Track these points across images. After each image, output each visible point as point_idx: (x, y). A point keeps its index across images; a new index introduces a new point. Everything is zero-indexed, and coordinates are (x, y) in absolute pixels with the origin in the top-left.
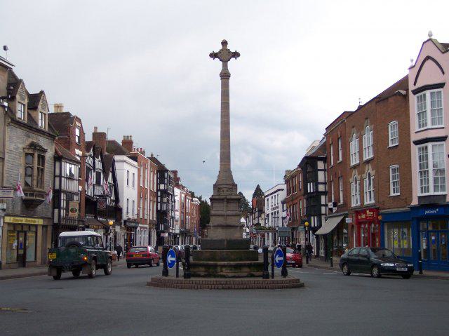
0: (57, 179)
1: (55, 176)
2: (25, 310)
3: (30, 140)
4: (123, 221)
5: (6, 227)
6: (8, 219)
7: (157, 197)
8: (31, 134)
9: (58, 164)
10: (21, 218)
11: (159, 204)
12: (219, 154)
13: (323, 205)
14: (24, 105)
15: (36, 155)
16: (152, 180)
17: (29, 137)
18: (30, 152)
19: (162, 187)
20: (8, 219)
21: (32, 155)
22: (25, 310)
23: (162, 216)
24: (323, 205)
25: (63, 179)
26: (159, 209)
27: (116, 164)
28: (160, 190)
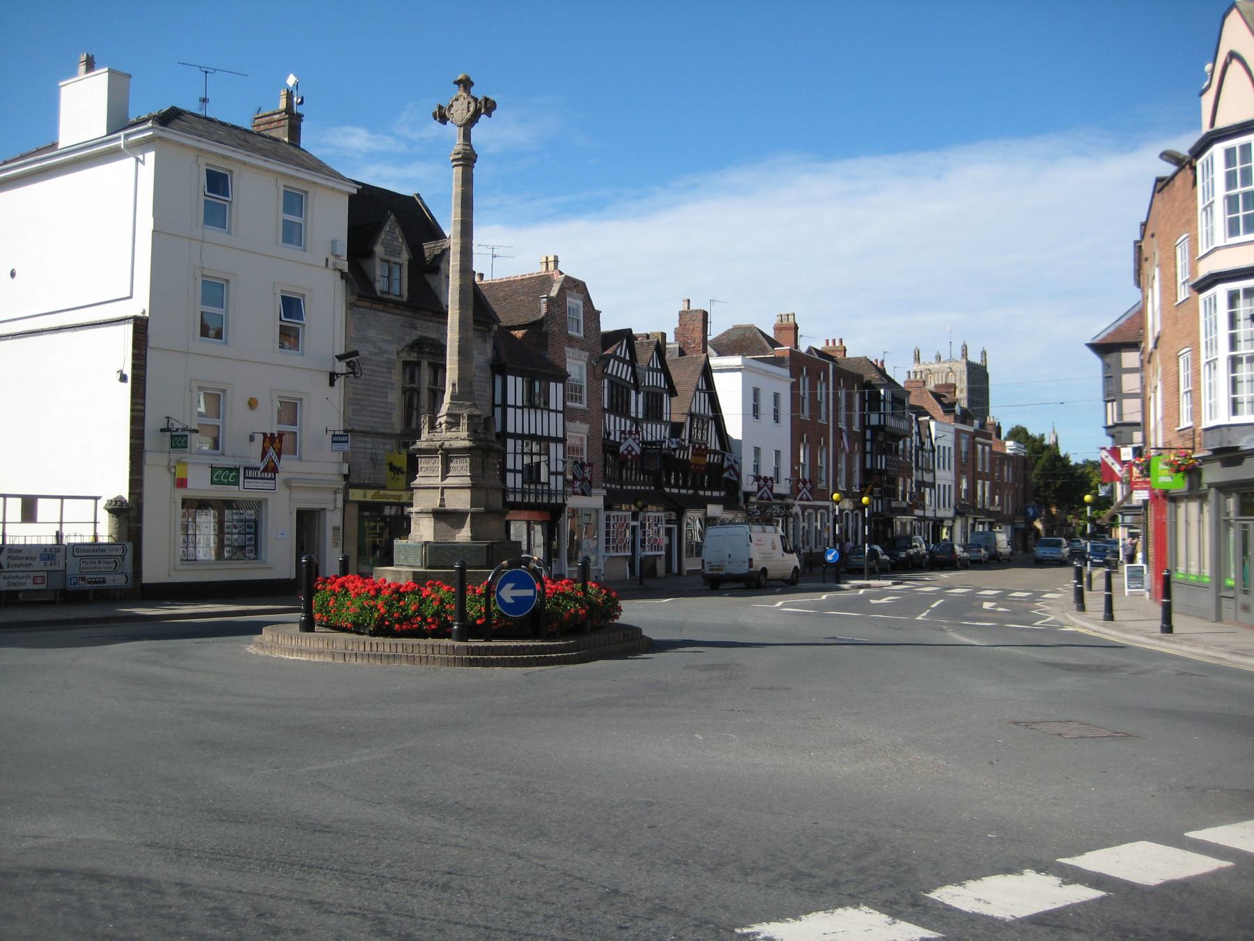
0: (498, 411)
1: (494, 406)
2: (37, 837)
3: (415, 335)
4: (741, 495)
5: (353, 512)
6: (356, 495)
7: (865, 441)
8: (418, 323)
9: (498, 379)
10: (399, 493)
11: (868, 457)
12: (518, 669)
13: (510, 471)
14: (401, 265)
15: (425, 364)
16: (843, 413)
17: (415, 328)
18: (413, 357)
19: (874, 419)
20: (356, 495)
21: (418, 364)
22: (37, 837)
23: (891, 886)
24: (510, 471)
25: (510, 411)
26: (868, 465)
27: (714, 375)
28: (870, 427)
